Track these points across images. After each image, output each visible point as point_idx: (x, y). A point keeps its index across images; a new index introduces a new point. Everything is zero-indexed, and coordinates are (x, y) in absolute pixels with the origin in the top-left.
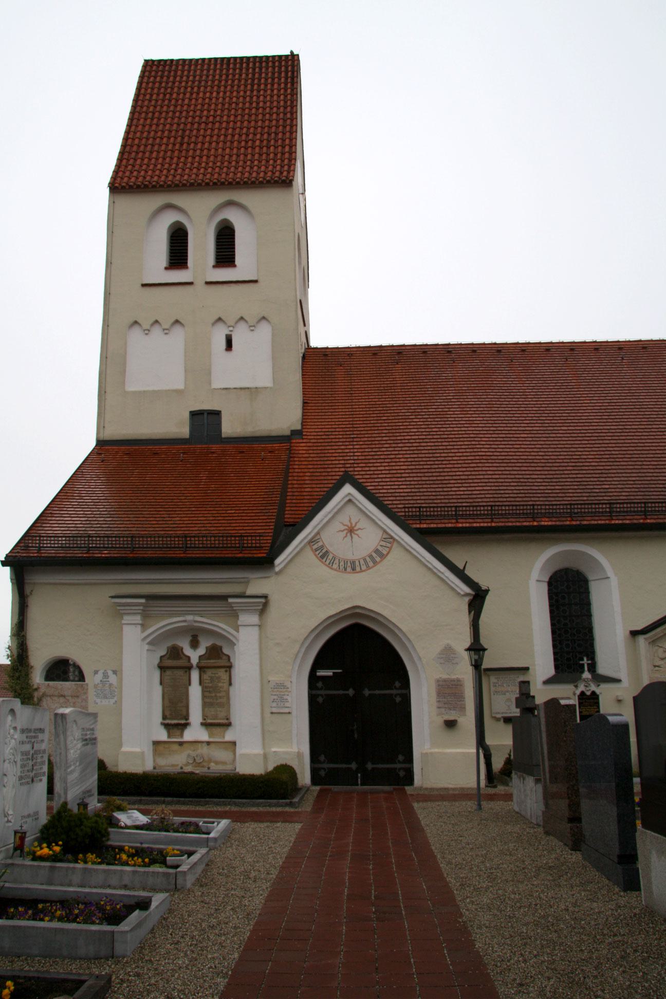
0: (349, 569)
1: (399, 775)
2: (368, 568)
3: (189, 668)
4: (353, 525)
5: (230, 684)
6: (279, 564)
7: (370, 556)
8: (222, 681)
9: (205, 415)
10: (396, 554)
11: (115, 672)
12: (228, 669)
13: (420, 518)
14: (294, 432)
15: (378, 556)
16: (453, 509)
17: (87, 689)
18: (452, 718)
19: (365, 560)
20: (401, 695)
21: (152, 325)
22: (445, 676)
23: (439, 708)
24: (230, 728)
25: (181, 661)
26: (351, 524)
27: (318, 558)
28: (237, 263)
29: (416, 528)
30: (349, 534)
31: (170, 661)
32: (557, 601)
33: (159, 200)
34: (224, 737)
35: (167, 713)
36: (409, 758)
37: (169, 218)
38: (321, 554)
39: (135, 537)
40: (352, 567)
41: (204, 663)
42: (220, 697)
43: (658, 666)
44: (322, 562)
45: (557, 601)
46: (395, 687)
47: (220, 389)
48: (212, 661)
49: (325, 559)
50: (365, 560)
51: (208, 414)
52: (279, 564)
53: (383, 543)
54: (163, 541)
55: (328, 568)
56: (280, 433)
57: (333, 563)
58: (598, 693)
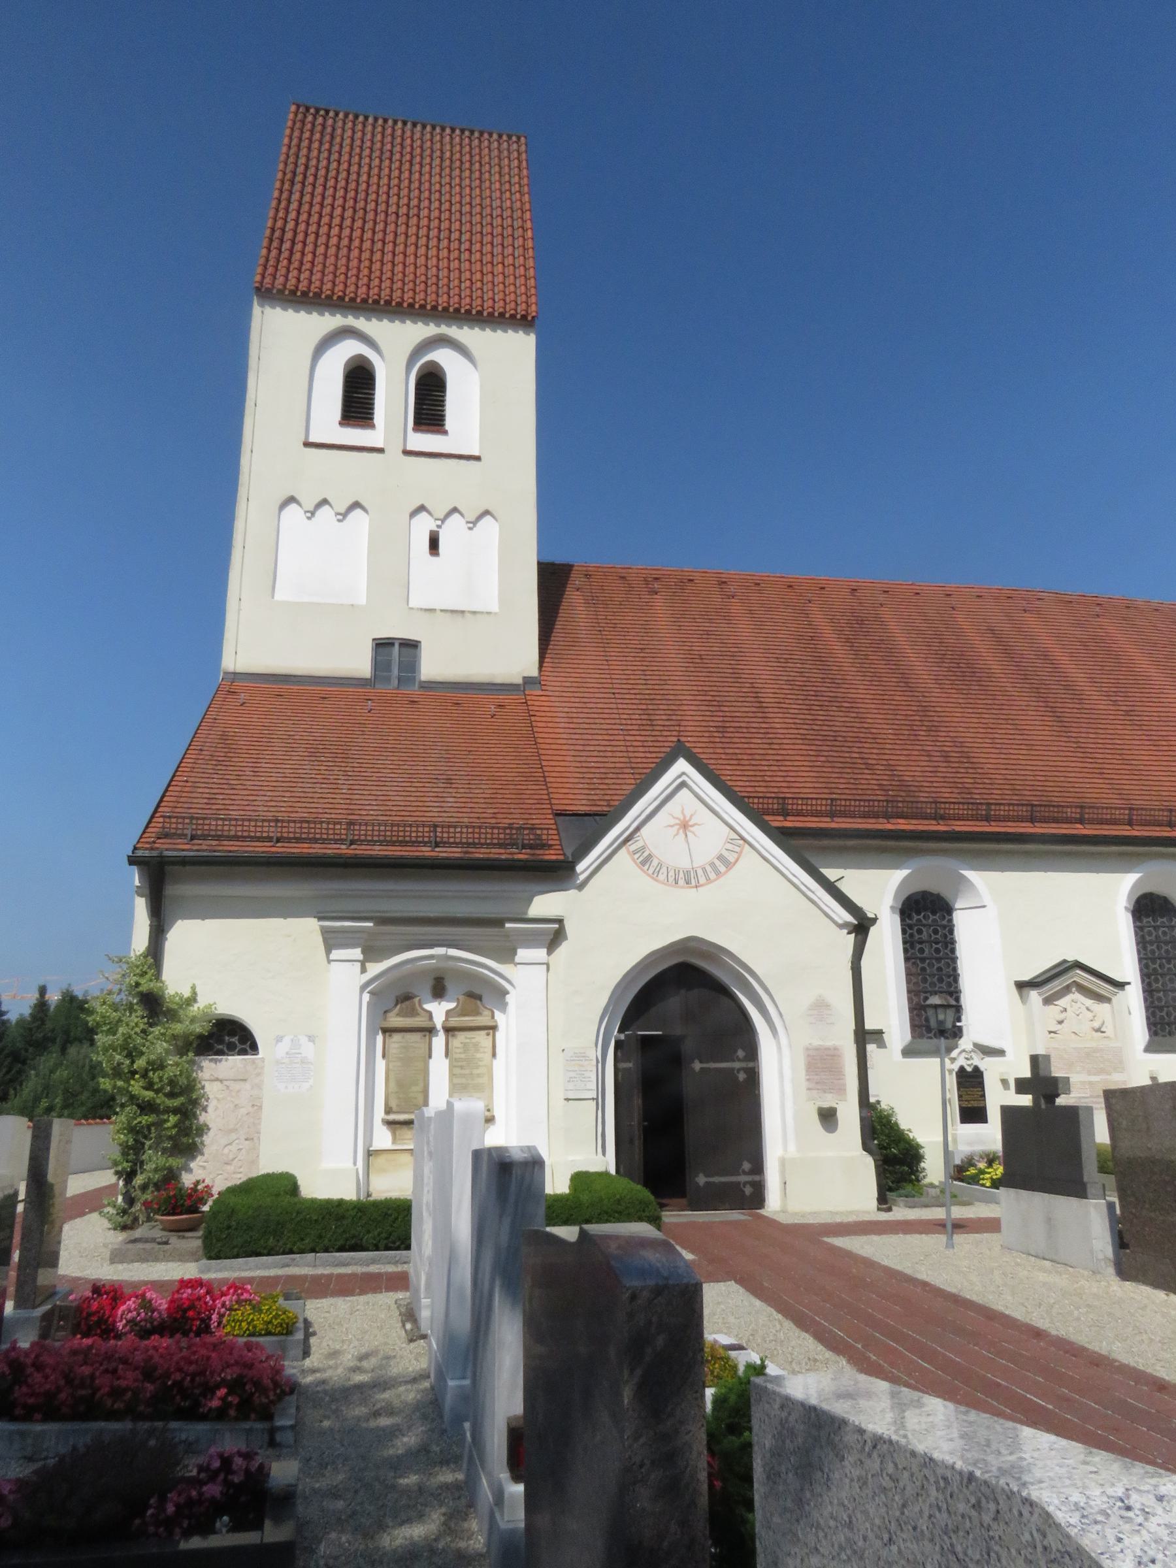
1: (744, 1192)
2: (709, 881)
3: (430, 1031)
5: (494, 1055)
6: (583, 872)
7: (712, 864)
8: (482, 1050)
9: (397, 646)
10: (749, 859)
11: (311, 1038)
12: (491, 1031)
13: (785, 813)
14: (528, 681)
15: (723, 864)
16: (829, 802)
17: (262, 1068)
20: (746, 1070)
21: (414, 514)
22: (817, 1043)
23: (809, 1089)
24: (494, 1124)
25: (417, 1019)
27: (636, 863)
28: (449, 424)
29: (778, 828)
30: (681, 831)
31: (401, 1019)
32: (911, 935)
33: (331, 321)
35: (393, 1104)
36: (758, 1167)
37: (349, 349)
38: (641, 859)
39: (354, 824)
40: (689, 879)
41: (455, 1021)
42: (479, 1075)
43: (1055, 1032)
44: (642, 870)
45: (911, 935)
47: (421, 609)
49: (646, 867)
50: (712, 864)
51: (401, 645)
52: (583, 872)
53: (730, 847)
54: (492, 834)
55: (651, 880)
58: (982, 1069)
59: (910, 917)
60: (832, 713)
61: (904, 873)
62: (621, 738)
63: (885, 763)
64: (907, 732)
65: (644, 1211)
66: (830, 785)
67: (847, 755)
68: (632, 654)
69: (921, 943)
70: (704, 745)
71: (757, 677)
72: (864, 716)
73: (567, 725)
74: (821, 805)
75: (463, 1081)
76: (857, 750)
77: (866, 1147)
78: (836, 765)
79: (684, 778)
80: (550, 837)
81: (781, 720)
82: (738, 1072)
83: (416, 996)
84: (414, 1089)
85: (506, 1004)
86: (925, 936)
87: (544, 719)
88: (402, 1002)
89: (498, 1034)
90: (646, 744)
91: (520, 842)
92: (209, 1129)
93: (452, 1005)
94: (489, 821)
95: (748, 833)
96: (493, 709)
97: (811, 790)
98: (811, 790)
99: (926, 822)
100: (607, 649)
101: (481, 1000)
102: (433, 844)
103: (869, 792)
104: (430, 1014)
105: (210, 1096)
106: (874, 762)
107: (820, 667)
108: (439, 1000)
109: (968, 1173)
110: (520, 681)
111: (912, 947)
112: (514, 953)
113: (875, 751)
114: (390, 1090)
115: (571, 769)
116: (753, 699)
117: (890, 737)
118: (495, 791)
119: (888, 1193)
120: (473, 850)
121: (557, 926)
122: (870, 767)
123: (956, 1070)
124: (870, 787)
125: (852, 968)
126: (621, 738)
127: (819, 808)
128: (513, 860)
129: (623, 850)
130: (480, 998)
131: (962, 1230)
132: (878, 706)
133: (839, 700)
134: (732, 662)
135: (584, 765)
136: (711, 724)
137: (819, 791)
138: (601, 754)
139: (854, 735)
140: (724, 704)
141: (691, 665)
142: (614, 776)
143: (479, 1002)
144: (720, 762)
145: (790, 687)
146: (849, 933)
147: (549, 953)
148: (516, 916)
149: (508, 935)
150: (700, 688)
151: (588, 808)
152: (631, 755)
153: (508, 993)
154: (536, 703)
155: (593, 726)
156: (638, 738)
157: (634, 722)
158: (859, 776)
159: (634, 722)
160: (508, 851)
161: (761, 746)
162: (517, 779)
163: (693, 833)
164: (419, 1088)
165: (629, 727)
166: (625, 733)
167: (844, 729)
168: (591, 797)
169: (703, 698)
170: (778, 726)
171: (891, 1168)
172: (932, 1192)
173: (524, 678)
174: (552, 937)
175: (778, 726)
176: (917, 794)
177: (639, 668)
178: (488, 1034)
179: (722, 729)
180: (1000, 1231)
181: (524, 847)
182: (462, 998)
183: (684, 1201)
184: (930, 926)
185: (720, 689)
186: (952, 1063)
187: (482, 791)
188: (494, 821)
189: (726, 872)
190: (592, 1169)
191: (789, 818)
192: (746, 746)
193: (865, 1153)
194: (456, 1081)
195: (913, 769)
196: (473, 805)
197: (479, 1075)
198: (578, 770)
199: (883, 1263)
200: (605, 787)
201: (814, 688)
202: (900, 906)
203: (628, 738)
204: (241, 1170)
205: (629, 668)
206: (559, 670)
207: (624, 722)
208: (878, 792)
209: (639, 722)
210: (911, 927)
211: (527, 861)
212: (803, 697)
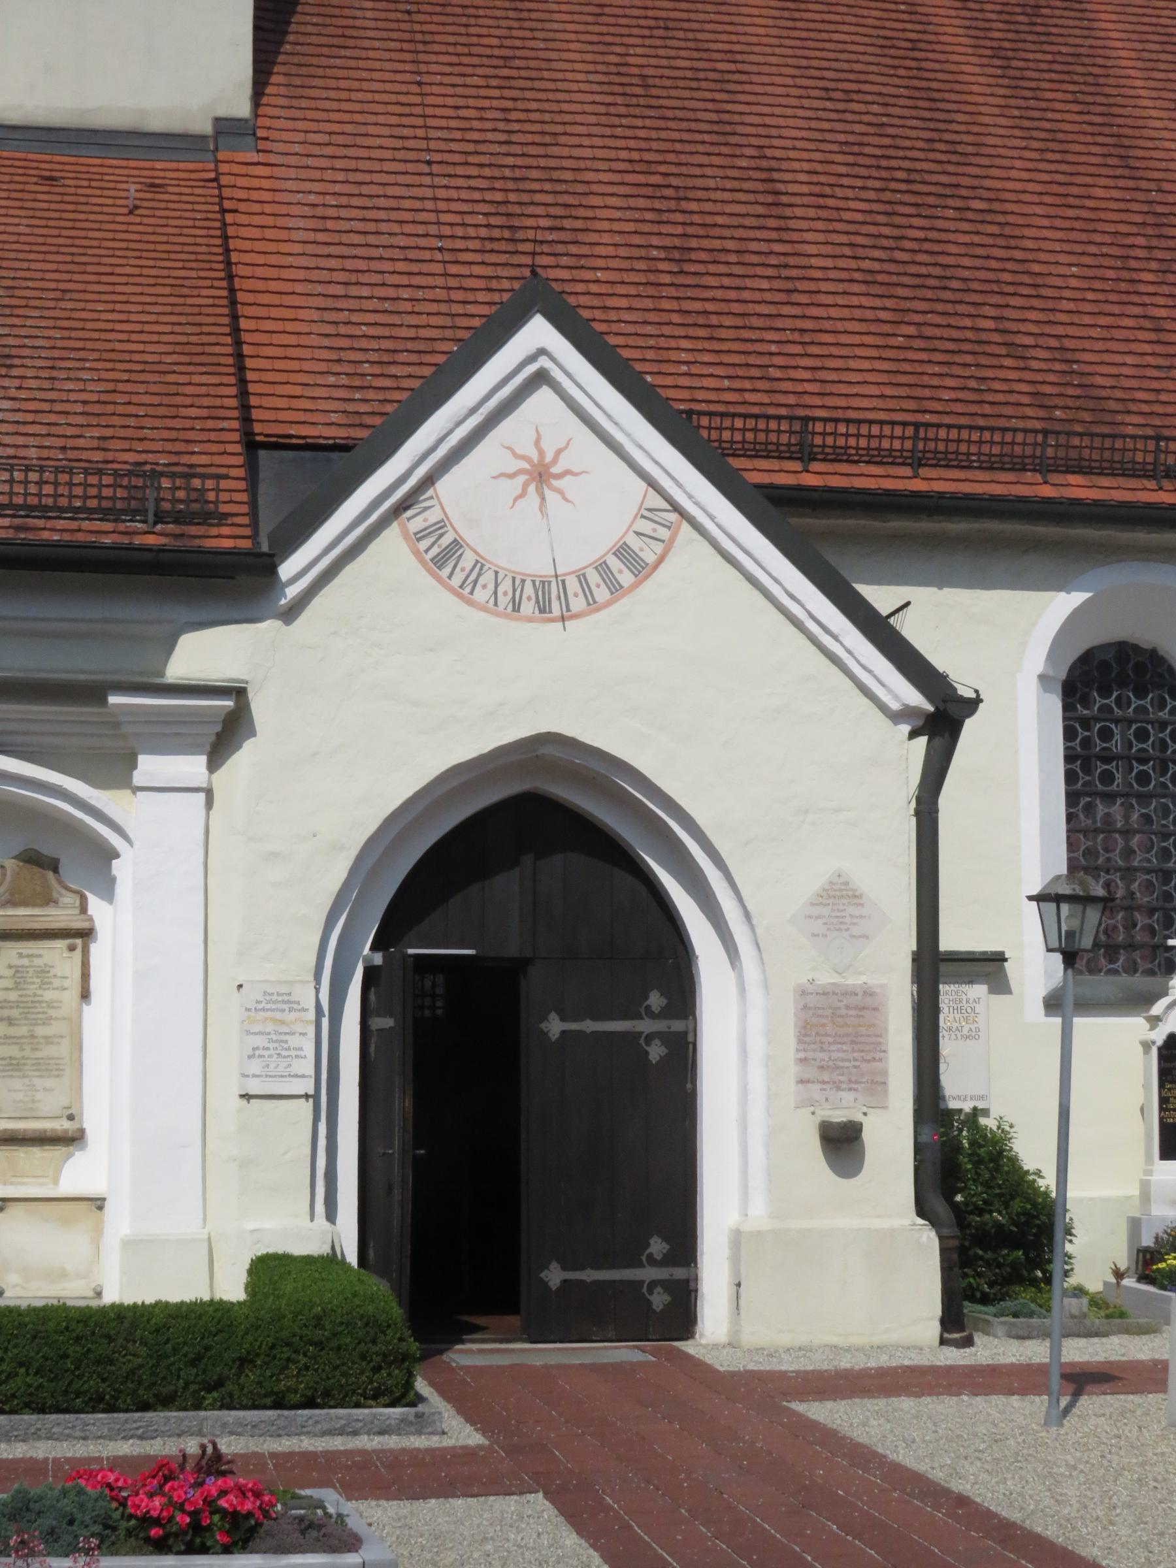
0: (528, 607)
1: (649, 1303)
2: (593, 606)
4: (549, 458)
5: (85, 995)
7: (602, 567)
8: (56, 983)
12: (79, 941)
14: (226, 128)
16: (910, 431)
18: (839, 1116)
19: (582, 578)
22: (826, 978)
23: (801, 1082)
24: (83, 1148)
26: (541, 453)
27: (421, 561)
29: (758, 486)
30: (532, 488)
32: (1086, 743)
34: (56, 1181)
38: (435, 550)
42: (48, 1040)
44: (439, 579)
45: (1086, 743)
46: (648, 1008)
48: (22, 911)
49: (447, 570)
50: (602, 567)
53: (645, 526)
56: (177, 125)
57: (476, 582)
59: (1086, 701)
60: (940, 224)
61: (1076, 598)
62: (438, 268)
63: (1054, 343)
64: (1111, 274)
65: (374, 1342)
66: (919, 392)
67: (968, 322)
68: (480, 71)
69: (1107, 760)
70: (632, 290)
71: (774, 132)
72: (1017, 232)
73: (311, 236)
74: (732, 429)
76: (991, 312)
77: (922, 1209)
78: (939, 344)
79: (543, 362)
80: (224, 496)
81: (821, 237)
82: (648, 1043)
85: (113, 880)
86: (1116, 745)
87: (257, 220)
89: (94, 948)
90: (494, 284)
91: (151, 507)
94: (85, 455)
95: (690, 497)
96: (132, 193)
97: (874, 403)
98: (874, 403)
99: (1133, 483)
100: (421, 57)
101: (56, 870)
102: (151, 518)
103: (1008, 411)
106: (1029, 341)
107: (927, 114)
109: (1162, 1265)
110: (208, 128)
111: (1087, 769)
112: (131, 763)
113: (1033, 315)
115: (313, 340)
116: (759, 186)
117: (1074, 283)
118: (111, 386)
119: (966, 1303)
120: (40, 523)
121: (229, 703)
122: (1019, 352)
123: (1160, 1042)
124: (1012, 398)
125: (918, 813)
126: (438, 268)
127: (886, 444)
128: (130, 548)
129: (393, 532)
130: (53, 865)
131: (1105, 1387)
132: (1053, 211)
133: (964, 192)
134: (718, 96)
135: (343, 330)
136: (655, 241)
137: (891, 404)
138: (387, 305)
139: (990, 276)
140: (691, 194)
141: (619, 100)
142: (414, 358)
143: (50, 875)
144: (667, 330)
145: (850, 159)
146: (913, 735)
147: (213, 766)
148: (124, 678)
149: (114, 723)
150: (635, 156)
151: (343, 433)
152: (457, 309)
153: (117, 855)
154: (241, 182)
155: (372, 239)
156: (477, 270)
157: (472, 232)
158: (990, 373)
159: (472, 232)
160: (121, 527)
161: (768, 296)
162: (168, 359)
163: (561, 492)
165: (460, 244)
166: (448, 256)
167: (966, 262)
168: (350, 407)
169: (641, 179)
170: (812, 249)
171: (989, 1255)
172: (1075, 1305)
173: (217, 120)
174: (218, 728)
175: (812, 249)
176: (1119, 418)
177: (495, 103)
178: (72, 949)
179: (680, 255)
180: (1165, 1391)
181: (160, 518)
183: (514, 1320)
184: (1130, 722)
185: (683, 158)
186: (1152, 1028)
187: (80, 385)
188: (98, 456)
189: (635, 586)
190: (299, 1249)
191: (815, 466)
192: (732, 295)
193: (920, 1221)
195: (1119, 359)
196: (52, 418)
198: (326, 342)
199: (892, 1457)
200: (388, 383)
201: (907, 164)
202: (1063, 675)
203: (453, 269)
205: (471, 102)
206: (304, 103)
207: (447, 231)
208: (1029, 412)
209: (483, 232)
210: (1086, 723)
211: (161, 550)
212: (878, 184)
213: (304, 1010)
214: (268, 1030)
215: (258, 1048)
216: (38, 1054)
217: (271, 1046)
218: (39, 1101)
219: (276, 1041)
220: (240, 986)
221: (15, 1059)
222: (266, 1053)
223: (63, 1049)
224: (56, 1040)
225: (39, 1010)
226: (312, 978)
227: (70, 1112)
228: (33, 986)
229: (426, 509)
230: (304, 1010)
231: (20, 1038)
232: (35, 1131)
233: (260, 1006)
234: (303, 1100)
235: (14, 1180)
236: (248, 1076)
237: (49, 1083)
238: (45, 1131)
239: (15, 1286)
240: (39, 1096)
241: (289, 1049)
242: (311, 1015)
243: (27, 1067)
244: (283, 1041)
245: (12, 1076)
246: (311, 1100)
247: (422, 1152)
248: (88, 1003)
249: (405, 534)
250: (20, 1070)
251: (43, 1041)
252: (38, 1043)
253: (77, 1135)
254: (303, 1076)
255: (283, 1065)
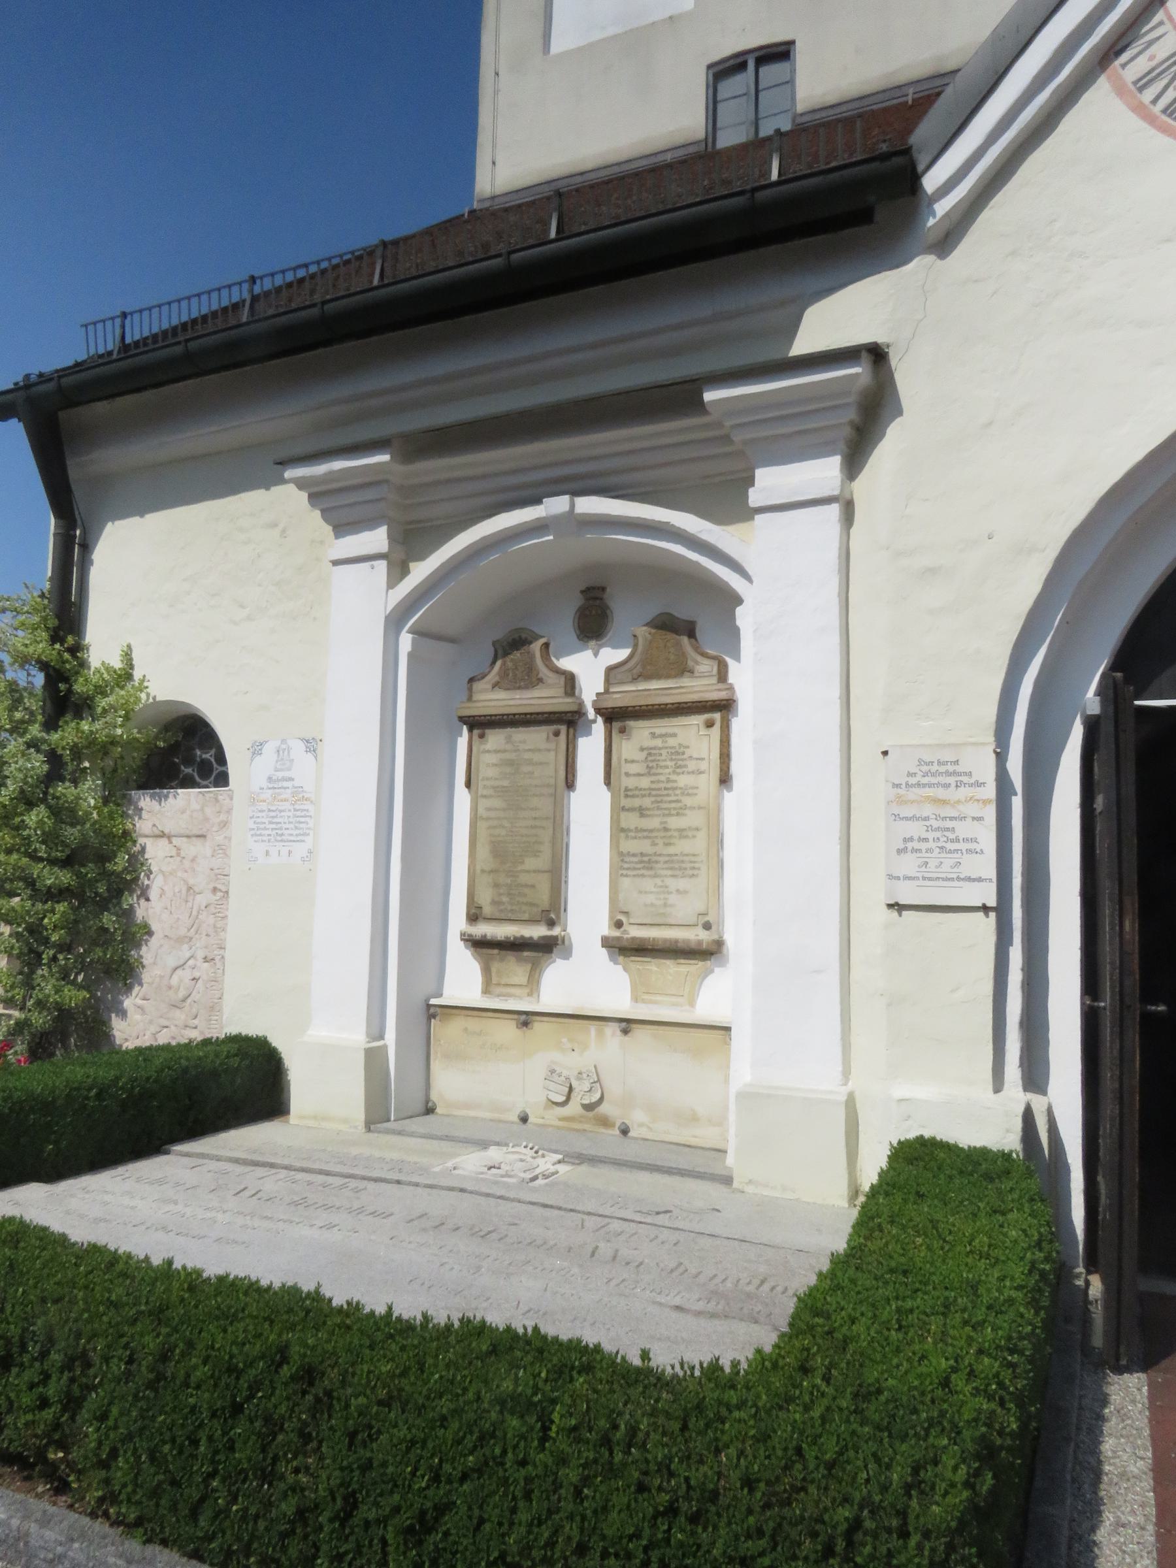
5: (725, 779)
8: (692, 765)
11: (312, 745)
12: (717, 716)
17: (229, 811)
24: (723, 963)
27: (1150, 119)
34: (692, 1003)
35: (485, 898)
41: (628, 693)
42: (682, 833)
48: (654, 685)
75: (644, 846)
83: (537, 637)
84: (531, 863)
85: (735, 632)
88: (506, 654)
89: (736, 724)
92: (150, 933)
93: (622, 654)
101: (691, 634)
104: (570, 681)
105: (154, 869)
108: (592, 643)
114: (478, 868)
129: (1100, 93)
130: (690, 630)
143: (685, 640)
153: (738, 600)
164: (541, 862)
174: (852, 414)
178: (710, 724)
182: (643, 632)
194: (630, 846)
197: (682, 833)
204: (196, 1022)
213: (979, 784)
214: (925, 814)
215: (911, 839)
216: (671, 850)
217: (931, 835)
218: (671, 906)
219: (938, 829)
220: (885, 753)
221: (646, 855)
222: (923, 846)
223: (698, 845)
224: (690, 834)
225: (673, 798)
226: (991, 739)
227: (707, 918)
228: (667, 771)
229: (1150, 44)
230: (979, 784)
231: (651, 831)
232: (665, 940)
233: (913, 781)
234: (980, 915)
235: (646, 997)
236: (898, 878)
237: (682, 884)
238: (676, 941)
239: (641, 1125)
240: (673, 899)
241: (957, 840)
242: (990, 792)
243: (659, 866)
244: (948, 829)
245: (643, 876)
246: (993, 915)
247: (1162, 1008)
248: (730, 789)
249: (1120, 90)
250: (651, 868)
251: (676, 834)
252: (671, 837)
253: (713, 948)
254: (980, 880)
255: (948, 863)
